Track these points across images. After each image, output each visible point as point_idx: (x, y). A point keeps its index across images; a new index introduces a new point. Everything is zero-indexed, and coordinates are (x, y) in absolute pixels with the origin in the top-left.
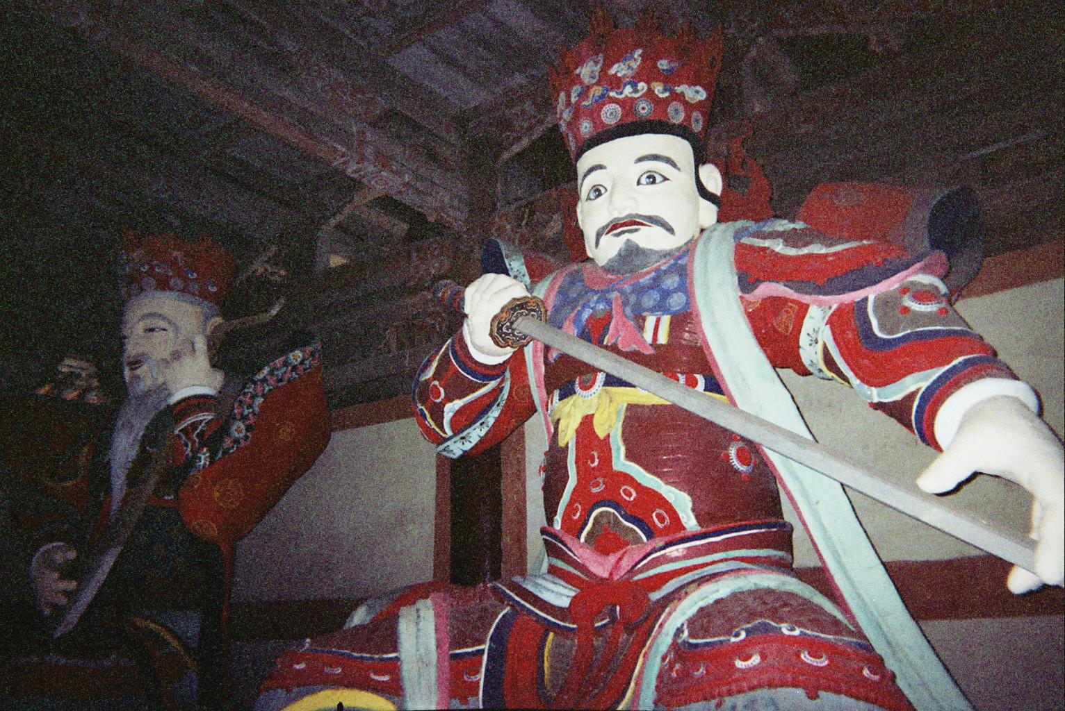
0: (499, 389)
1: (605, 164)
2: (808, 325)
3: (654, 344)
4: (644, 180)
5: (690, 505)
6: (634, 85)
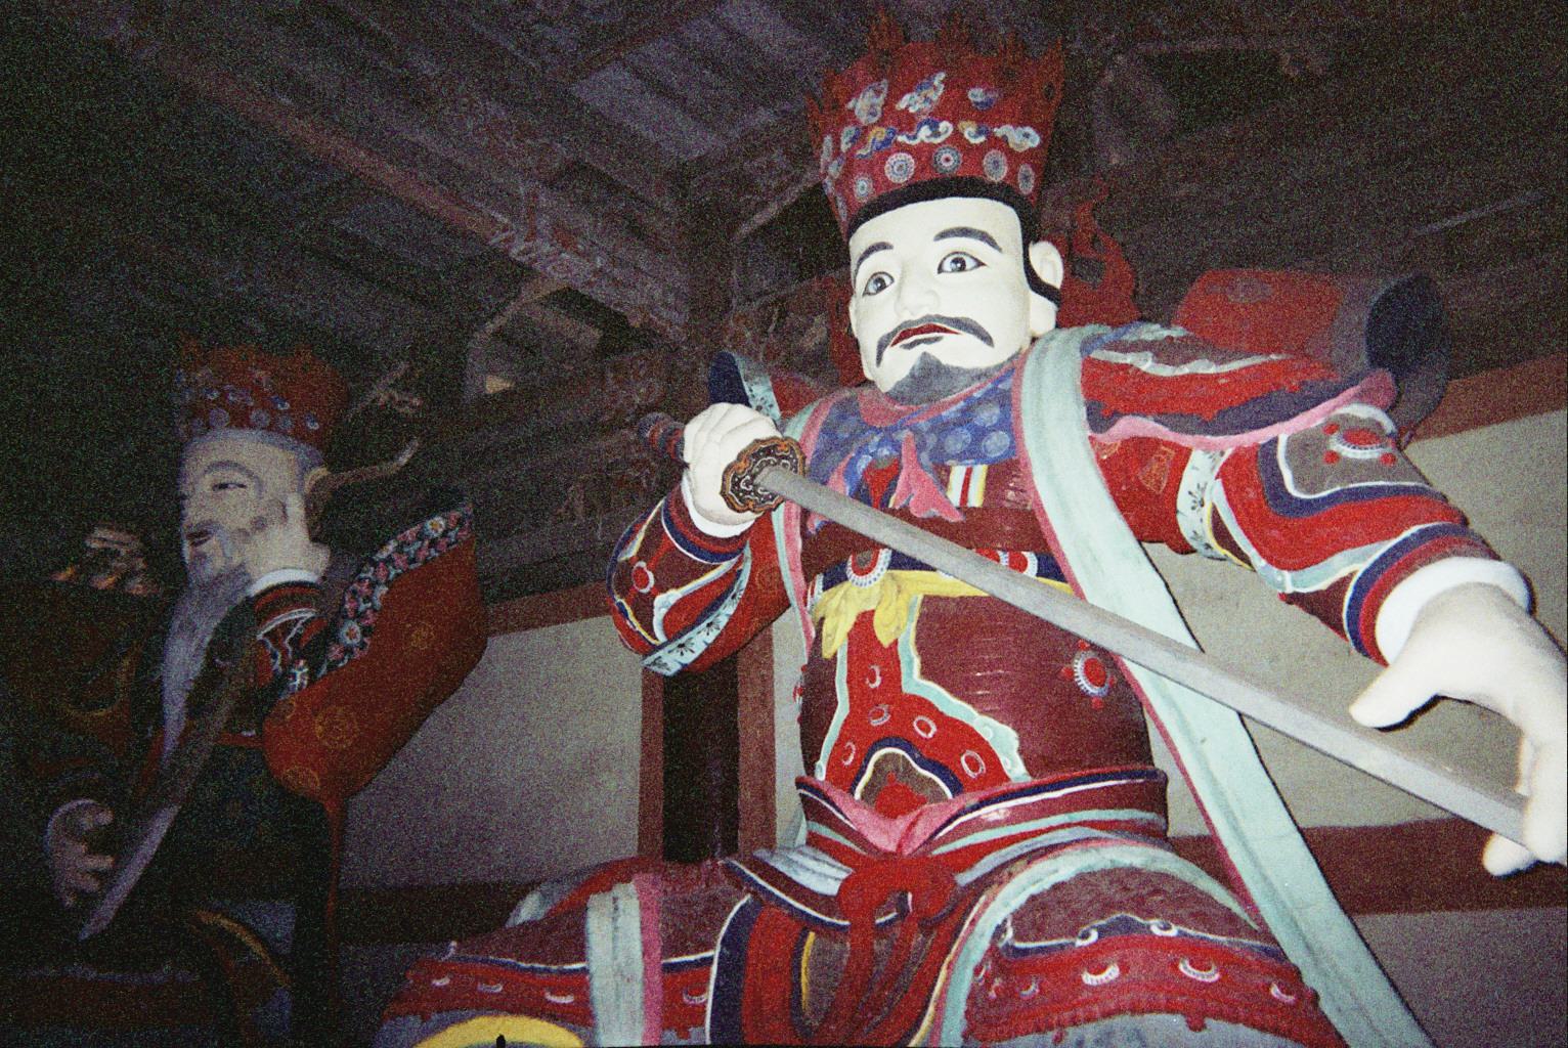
0: (734, 574)
1: (891, 242)
2: (1190, 479)
3: (963, 507)
4: (948, 266)
5: (1016, 744)
6: (934, 126)
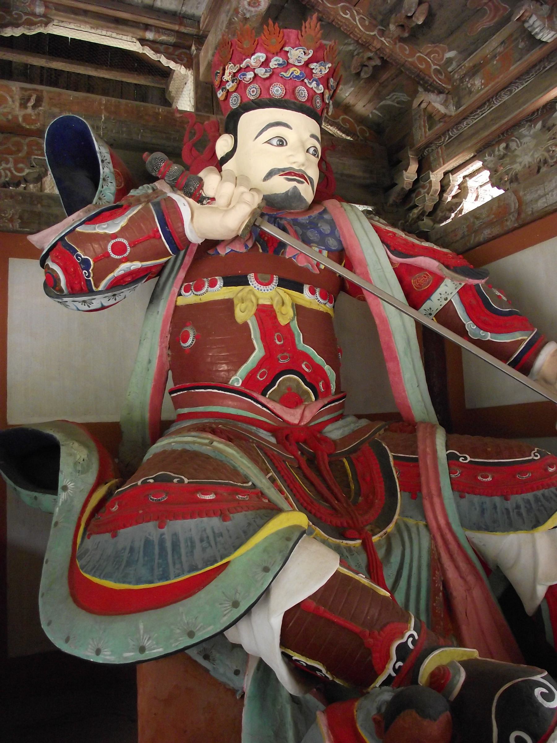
2: (442, 289)
6: (318, 85)
